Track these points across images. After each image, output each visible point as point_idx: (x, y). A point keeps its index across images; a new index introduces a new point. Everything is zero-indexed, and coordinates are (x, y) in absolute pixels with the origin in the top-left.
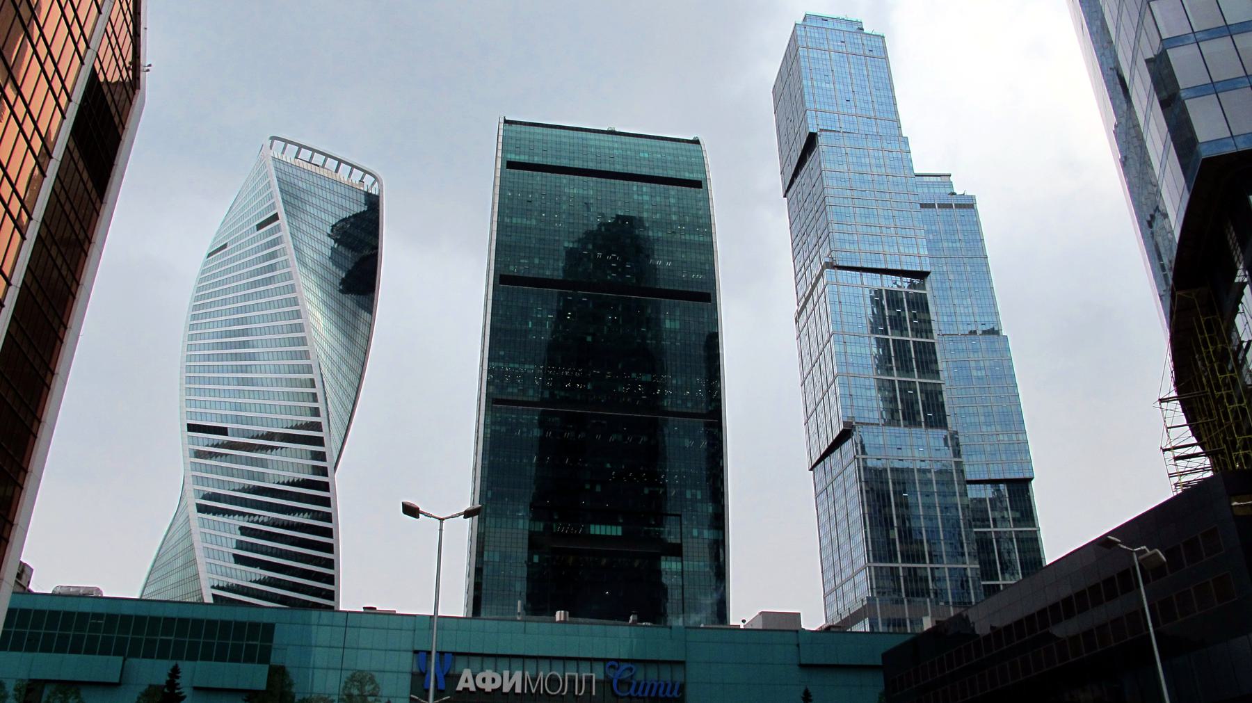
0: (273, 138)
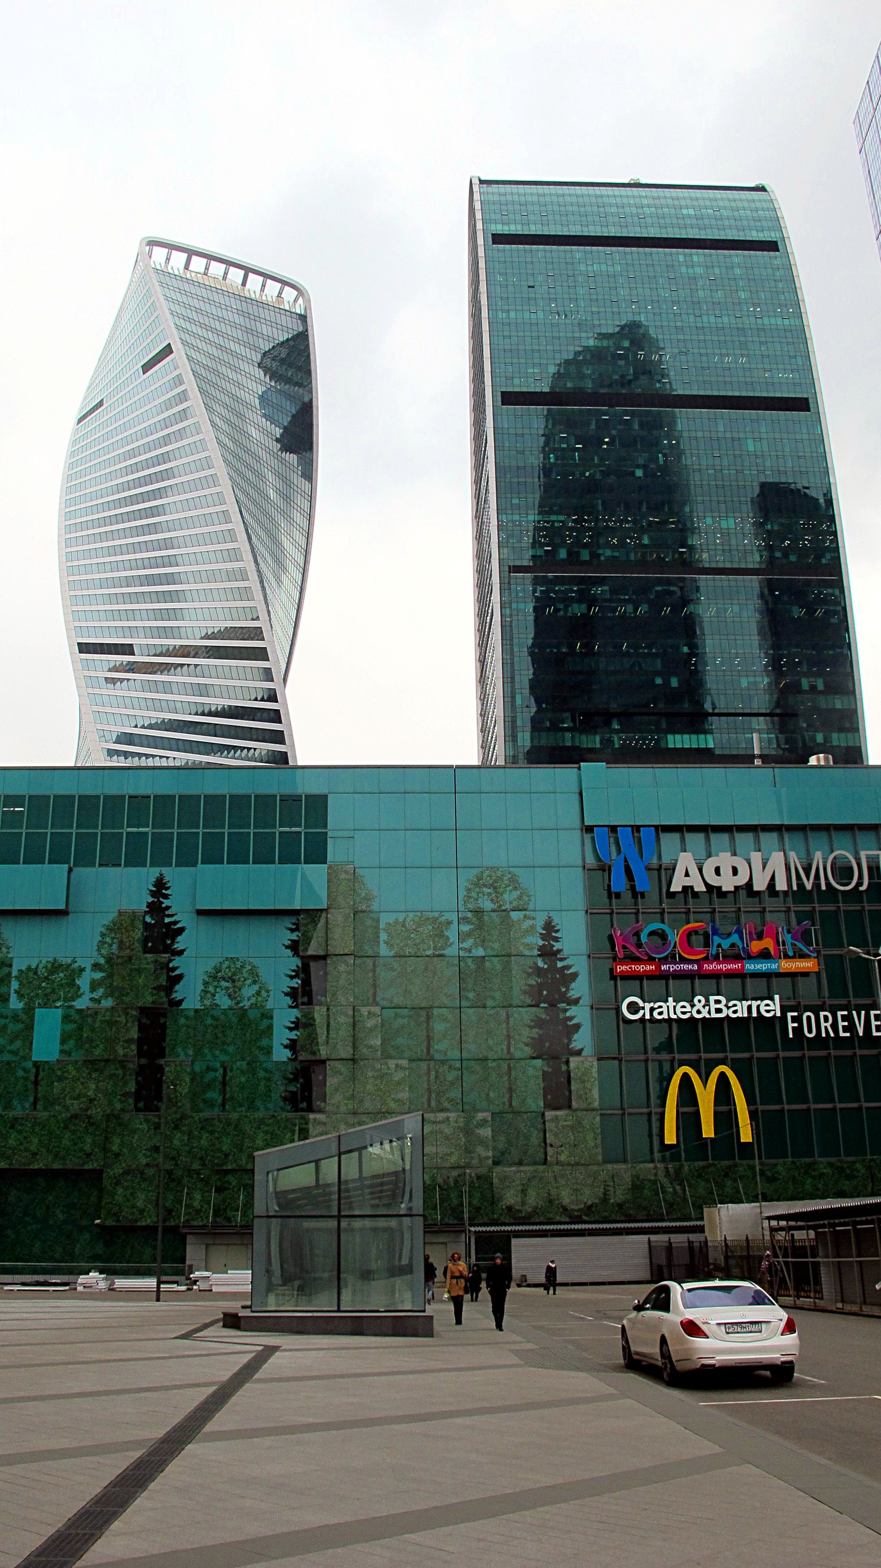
0: (153, 243)
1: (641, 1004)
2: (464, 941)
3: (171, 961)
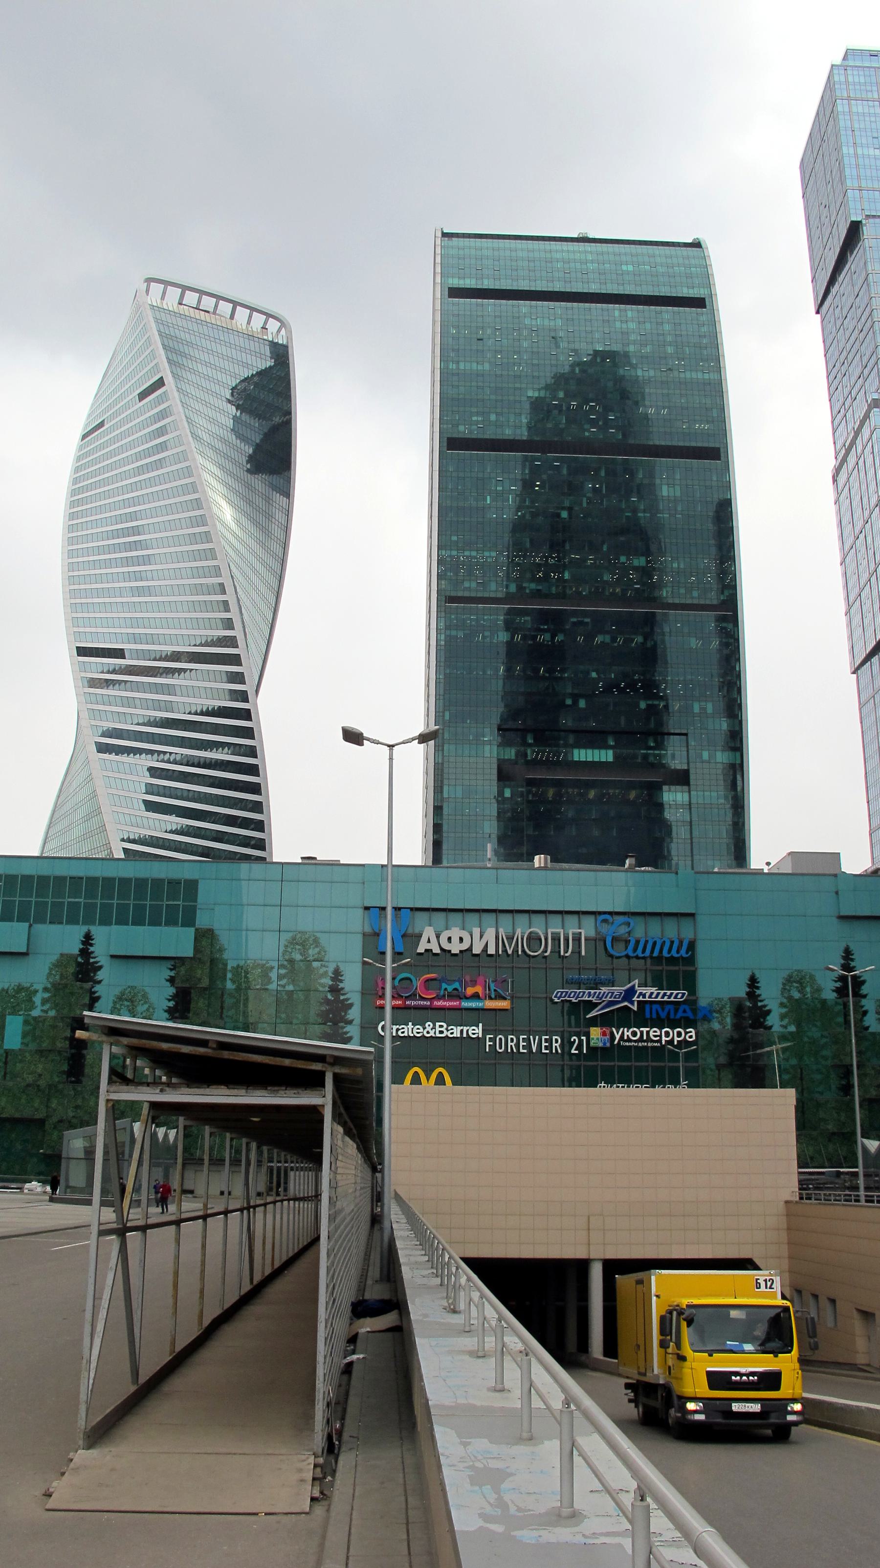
0: (149, 281)
2: (281, 980)
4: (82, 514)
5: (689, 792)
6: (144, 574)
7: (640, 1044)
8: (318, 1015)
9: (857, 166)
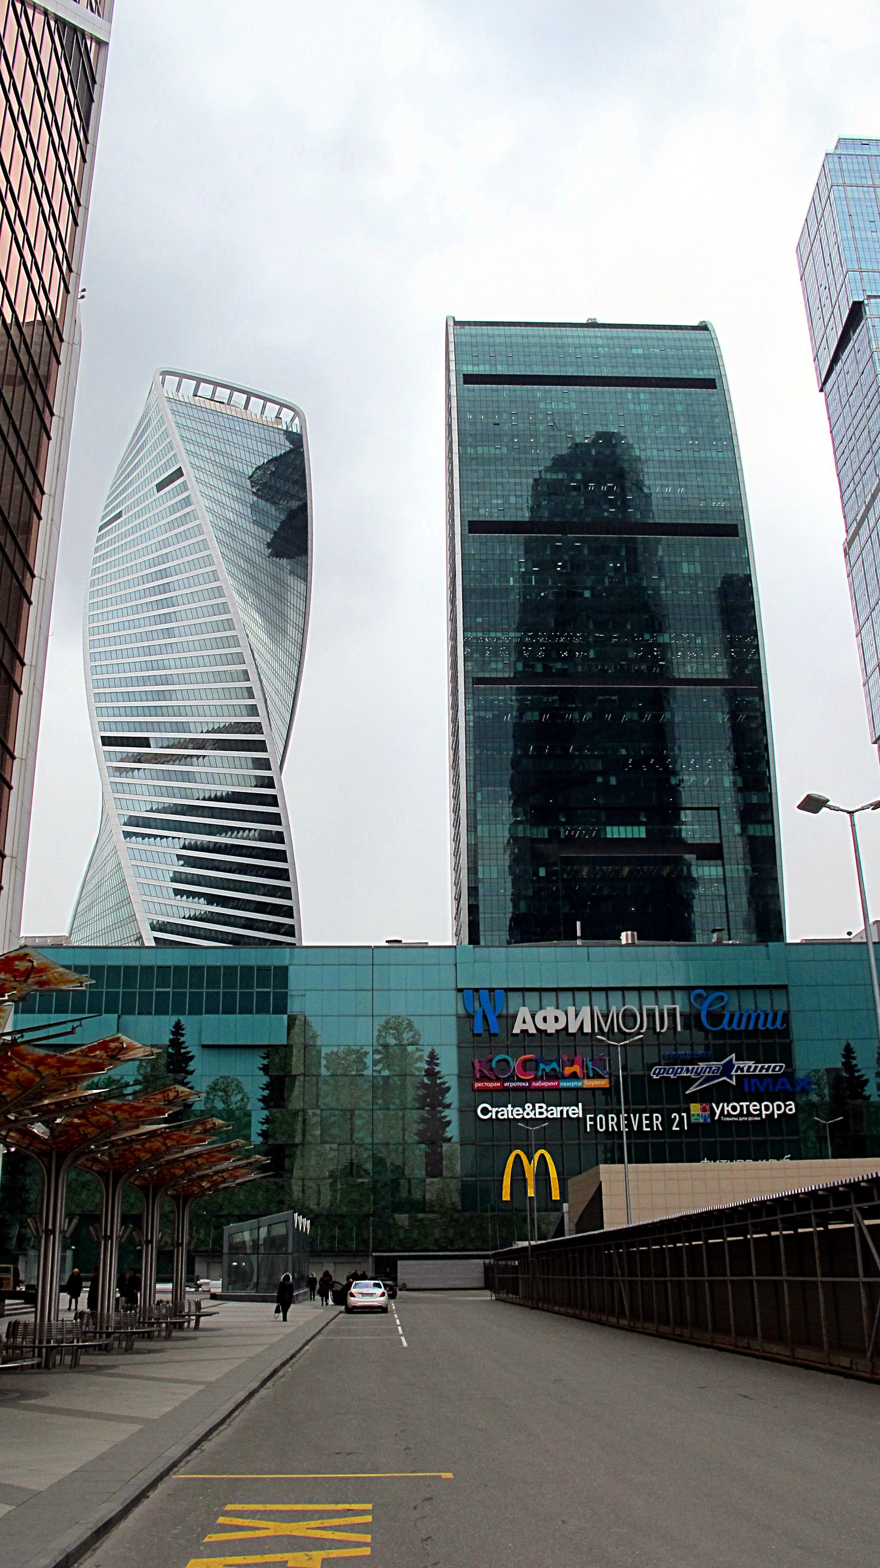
0: (165, 373)
1: (490, 1108)
3: (185, 1078)
4: (102, 605)
5: (723, 865)
6: (166, 662)
7: (741, 1119)
8: (415, 1100)
9: (856, 248)
